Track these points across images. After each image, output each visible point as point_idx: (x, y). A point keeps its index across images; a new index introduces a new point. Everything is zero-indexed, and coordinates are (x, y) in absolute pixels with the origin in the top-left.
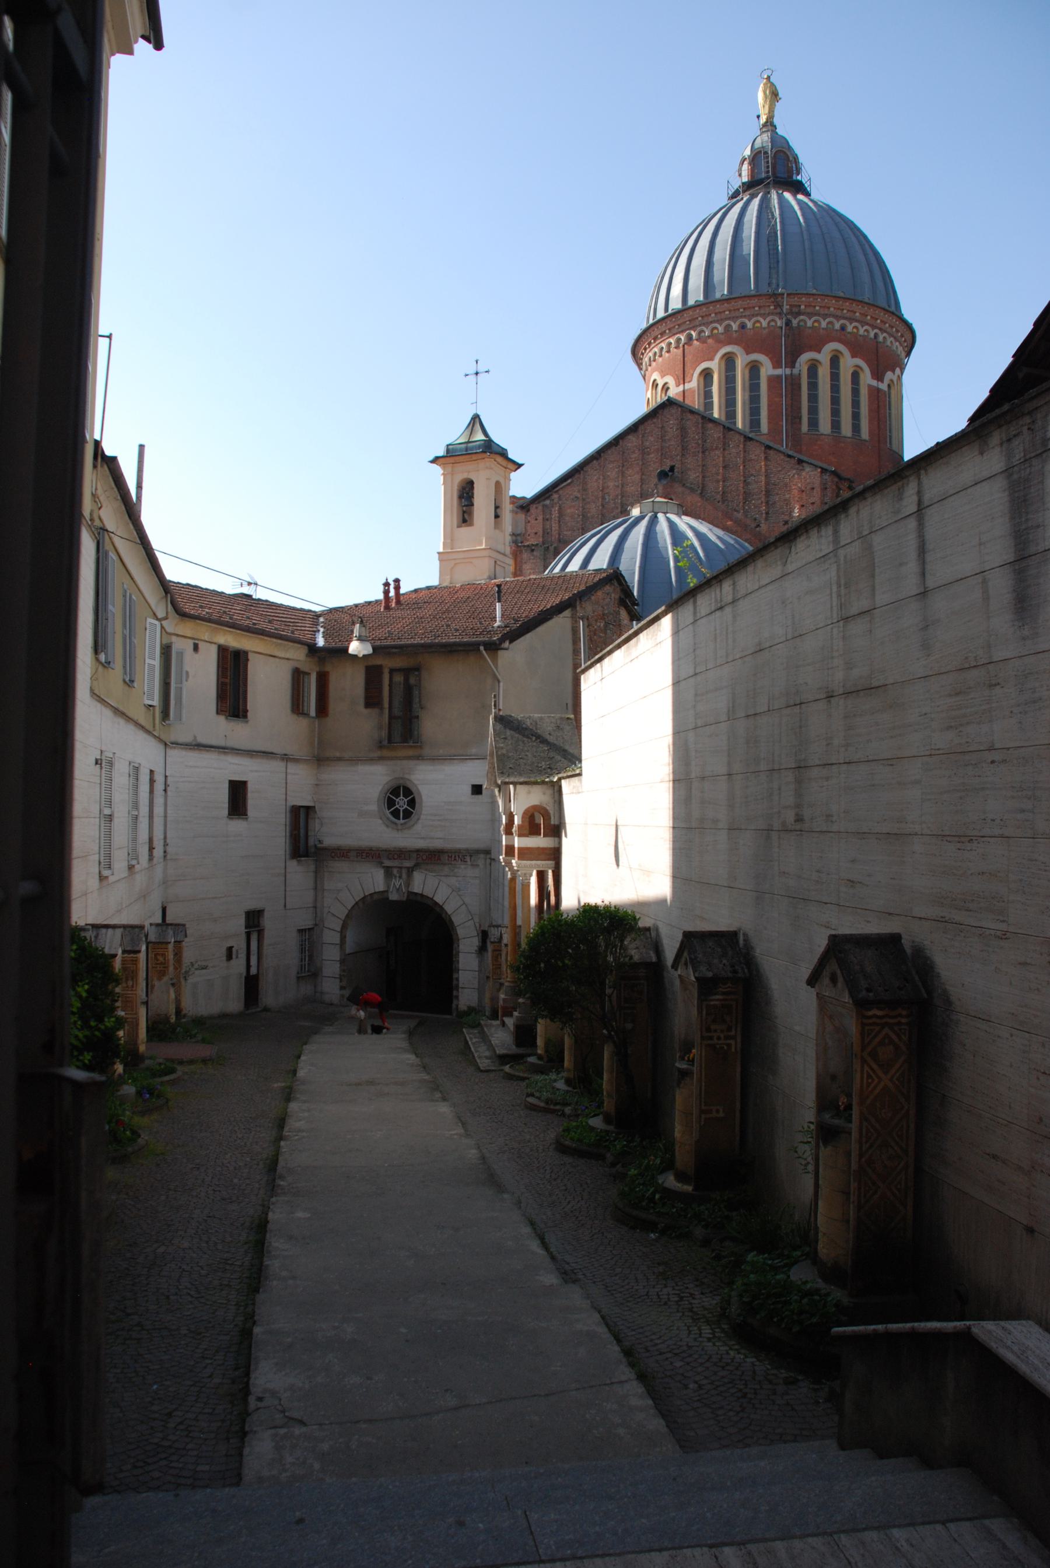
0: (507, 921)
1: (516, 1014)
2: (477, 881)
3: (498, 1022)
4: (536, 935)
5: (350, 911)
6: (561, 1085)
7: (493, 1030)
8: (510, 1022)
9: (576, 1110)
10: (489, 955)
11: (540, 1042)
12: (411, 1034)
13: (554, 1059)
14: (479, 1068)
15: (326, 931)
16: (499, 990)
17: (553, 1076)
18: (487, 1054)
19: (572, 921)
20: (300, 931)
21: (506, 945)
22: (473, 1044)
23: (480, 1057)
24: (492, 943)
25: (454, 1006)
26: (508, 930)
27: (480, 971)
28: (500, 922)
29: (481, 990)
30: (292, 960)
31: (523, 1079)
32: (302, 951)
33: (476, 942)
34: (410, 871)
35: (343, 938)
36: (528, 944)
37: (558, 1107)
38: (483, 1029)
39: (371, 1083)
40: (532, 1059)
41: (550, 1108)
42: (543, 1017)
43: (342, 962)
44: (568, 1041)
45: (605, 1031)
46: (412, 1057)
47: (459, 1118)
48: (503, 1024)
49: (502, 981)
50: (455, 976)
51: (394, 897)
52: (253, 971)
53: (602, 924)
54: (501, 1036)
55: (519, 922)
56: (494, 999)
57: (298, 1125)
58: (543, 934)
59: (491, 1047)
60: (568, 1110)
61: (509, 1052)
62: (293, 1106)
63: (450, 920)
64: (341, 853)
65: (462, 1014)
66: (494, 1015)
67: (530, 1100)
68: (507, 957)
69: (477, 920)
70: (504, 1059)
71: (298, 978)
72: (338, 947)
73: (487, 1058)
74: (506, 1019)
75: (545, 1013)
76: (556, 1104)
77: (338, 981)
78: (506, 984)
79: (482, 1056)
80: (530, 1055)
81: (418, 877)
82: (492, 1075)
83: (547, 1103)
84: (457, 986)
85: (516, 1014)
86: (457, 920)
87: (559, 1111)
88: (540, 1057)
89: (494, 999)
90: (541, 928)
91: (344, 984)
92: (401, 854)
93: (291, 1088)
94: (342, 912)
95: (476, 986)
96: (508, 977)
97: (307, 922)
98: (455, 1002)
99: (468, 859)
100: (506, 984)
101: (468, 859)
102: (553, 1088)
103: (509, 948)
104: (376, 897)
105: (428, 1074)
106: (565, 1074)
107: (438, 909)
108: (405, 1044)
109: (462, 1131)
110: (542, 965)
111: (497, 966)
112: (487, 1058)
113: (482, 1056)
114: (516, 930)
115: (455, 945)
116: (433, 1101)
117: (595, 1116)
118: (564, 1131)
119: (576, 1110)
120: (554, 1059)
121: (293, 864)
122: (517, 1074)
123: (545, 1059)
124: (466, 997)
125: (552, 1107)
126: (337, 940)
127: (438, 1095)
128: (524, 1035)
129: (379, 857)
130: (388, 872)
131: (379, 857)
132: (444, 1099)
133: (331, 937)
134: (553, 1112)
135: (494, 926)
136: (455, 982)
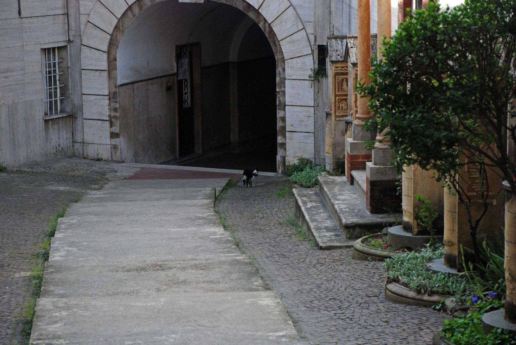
0: (355, 30)
1: (370, 165)
3: (344, 178)
4: (399, 39)
5: (120, 20)
6: (439, 265)
7: (336, 189)
8: (361, 177)
9: (463, 302)
10: (329, 82)
11: (407, 205)
12: (217, 199)
13: (430, 229)
14: (317, 245)
15: (85, 51)
16: (344, 133)
17: (427, 252)
18: (329, 223)
19: (455, 16)
20: (47, 51)
21: (355, 65)
22: (307, 209)
23: (318, 229)
24: (332, 62)
25: (279, 158)
26: (357, 42)
27: (316, 107)
28: (345, 32)
29: (318, 135)
31: (382, 258)
32: (50, 80)
33: (310, 63)
35: (112, 61)
36: (387, 54)
37: (435, 298)
38: (321, 189)
39: (160, 267)
40: (396, 230)
41: (424, 299)
42: (411, 162)
43: (112, 97)
44: (449, 201)
45: (505, 183)
46: (219, 231)
47: (289, 314)
48: (352, 181)
49: (349, 118)
50: (280, 114)
52: (188, 104)
53: (503, 18)
54: (350, 199)
55: (374, 30)
56: (338, 146)
57: (52, 328)
58: (409, 38)
59: (335, 214)
60: (450, 302)
61: (361, 221)
62: (44, 302)
63: (271, 31)
65: (289, 171)
66: (339, 169)
67: (394, 287)
68: (356, 76)
69: (310, 30)
70: (354, 230)
71: (46, 121)
72: (105, 74)
73: (328, 229)
74: (354, 173)
75: (413, 156)
76: (432, 293)
77: (107, 124)
78: (356, 122)
79: (322, 227)
80: (391, 225)
82: (336, 253)
83: (419, 292)
84: (284, 128)
85: (370, 165)
86: (280, 31)
87: (436, 303)
88: (407, 227)
89: (338, 146)
90: (406, 28)
91: (116, 129)
93: (40, 278)
95: (311, 129)
96: (358, 106)
97: (57, 39)
98: (280, 153)
100: (356, 122)
102: (428, 270)
103: (359, 68)
105: (244, 253)
106: (444, 250)
107: (251, 15)
108: (209, 213)
109: (294, 332)
110: (409, 86)
111: (342, 98)
112: (328, 229)
113: (322, 227)
114: (368, 40)
115: (279, 69)
116: (251, 290)
117: (492, 309)
118: (445, 331)
119: (463, 302)
120: (430, 229)
122: (373, 251)
123: (416, 230)
124: (295, 146)
125: (426, 297)
126: (104, 65)
127: (257, 282)
128: (384, 196)
132: (267, 288)
133: (94, 59)
134: (427, 304)
135: (336, 38)
136: (279, 124)
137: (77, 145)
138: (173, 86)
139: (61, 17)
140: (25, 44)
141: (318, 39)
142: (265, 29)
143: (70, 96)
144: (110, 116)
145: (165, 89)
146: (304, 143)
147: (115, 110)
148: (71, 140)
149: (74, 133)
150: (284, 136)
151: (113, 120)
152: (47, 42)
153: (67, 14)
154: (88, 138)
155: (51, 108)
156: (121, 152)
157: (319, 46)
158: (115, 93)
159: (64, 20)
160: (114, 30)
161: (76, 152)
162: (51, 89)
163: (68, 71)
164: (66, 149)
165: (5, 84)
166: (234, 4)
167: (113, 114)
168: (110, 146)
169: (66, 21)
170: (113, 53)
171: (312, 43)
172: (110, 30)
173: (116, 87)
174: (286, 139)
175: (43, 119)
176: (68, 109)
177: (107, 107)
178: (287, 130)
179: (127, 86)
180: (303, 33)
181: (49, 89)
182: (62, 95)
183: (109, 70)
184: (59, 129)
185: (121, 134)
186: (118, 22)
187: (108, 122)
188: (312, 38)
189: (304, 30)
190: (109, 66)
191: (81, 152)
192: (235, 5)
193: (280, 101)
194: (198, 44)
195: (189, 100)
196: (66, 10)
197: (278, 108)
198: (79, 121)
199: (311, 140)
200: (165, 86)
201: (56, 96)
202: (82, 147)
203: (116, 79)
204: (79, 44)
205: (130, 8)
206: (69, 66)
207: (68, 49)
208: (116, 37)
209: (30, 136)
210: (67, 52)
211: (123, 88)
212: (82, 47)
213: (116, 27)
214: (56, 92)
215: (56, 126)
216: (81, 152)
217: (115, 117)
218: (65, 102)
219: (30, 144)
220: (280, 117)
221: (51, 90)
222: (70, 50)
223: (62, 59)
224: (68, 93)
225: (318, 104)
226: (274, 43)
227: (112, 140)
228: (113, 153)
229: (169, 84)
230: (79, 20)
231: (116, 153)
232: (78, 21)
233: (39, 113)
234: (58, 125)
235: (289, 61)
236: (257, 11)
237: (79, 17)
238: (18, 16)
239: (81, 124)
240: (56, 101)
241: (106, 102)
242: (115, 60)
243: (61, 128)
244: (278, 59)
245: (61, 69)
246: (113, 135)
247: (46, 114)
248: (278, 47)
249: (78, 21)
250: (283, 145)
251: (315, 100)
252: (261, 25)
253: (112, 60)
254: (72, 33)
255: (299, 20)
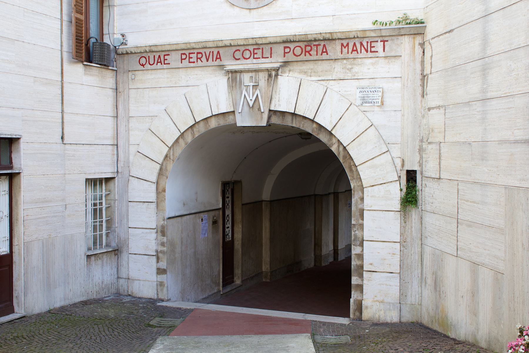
2: (397, 85)
15: (134, 182)
20: (94, 183)
30: (78, 226)
33: (396, 192)
34: (273, 75)
35: (160, 191)
43: (162, 231)
51: (243, 120)
52: (229, 238)
64: (155, 57)
71: (89, 257)
72: (154, 206)
77: (154, 259)
81: (287, 82)
84: (362, 267)
91: (163, 265)
92: (256, 48)
94: (159, 152)
99: (379, 46)
101: (379, 46)
104: (213, 124)
107: (323, 138)
121: (77, 71)
126: (152, 197)
129: (219, 58)
130: (234, 76)
131: (219, 58)
137: (121, 281)
138: (219, 219)
139: (110, 147)
140: (67, 172)
141: (406, 163)
142: (339, 153)
143: (116, 229)
144: (157, 251)
145: (211, 223)
146: (386, 285)
147: (163, 244)
148: (116, 276)
149: (119, 269)
150: (361, 276)
151: (160, 255)
152: (93, 171)
153: (117, 145)
154: (133, 274)
155: (95, 243)
156: (167, 290)
157: (408, 172)
158: (163, 227)
159: (113, 151)
160: (164, 159)
161: (120, 288)
162: (97, 222)
163: (114, 203)
164: (110, 286)
165: (40, 216)
166: (301, 126)
167: (160, 248)
168: (155, 283)
169: (115, 152)
170: (162, 184)
171: (399, 167)
172: (160, 159)
173: (164, 220)
174: (363, 280)
175: (85, 254)
176: (114, 244)
177: (154, 241)
178: (365, 269)
179: (175, 219)
180: (387, 156)
181: (94, 222)
182: (108, 228)
183: (157, 202)
184: (103, 265)
185: (168, 271)
186: (169, 151)
187: (154, 257)
188: (398, 162)
189: (388, 153)
190: (157, 198)
191: (126, 288)
192: (303, 127)
193: (355, 236)
194: (240, 182)
195: (230, 235)
196: (116, 141)
197: (353, 243)
198: (124, 256)
199: (395, 282)
200: (211, 220)
201: (101, 230)
202: (126, 283)
203: (164, 210)
204: (128, 175)
205: (182, 135)
206: (116, 198)
207: (116, 181)
208: (166, 167)
209: (68, 274)
210: (115, 184)
211: (171, 220)
212: (131, 178)
213: (166, 156)
214: (101, 226)
215: (99, 262)
216: (126, 288)
217: (162, 252)
218: (110, 235)
219: (68, 283)
220: (356, 254)
221: (96, 224)
222: (118, 181)
223: (110, 191)
224: (113, 226)
225: (406, 239)
226: (351, 170)
227: (158, 276)
228: (159, 291)
229: (215, 218)
230: (129, 150)
231: (162, 290)
232: (127, 151)
233: (81, 249)
234: (103, 261)
235: (370, 188)
236: (330, 133)
237: (129, 147)
238: (60, 140)
239: (127, 259)
240: (101, 236)
241: (153, 235)
242: (164, 191)
243: (105, 264)
244: (354, 187)
245: (108, 202)
246: (160, 271)
247: (89, 249)
248: (355, 173)
249: (127, 151)
250: (360, 288)
251: (401, 234)
252: (334, 149)
253: (160, 191)
254: (121, 164)
255: (382, 142)
